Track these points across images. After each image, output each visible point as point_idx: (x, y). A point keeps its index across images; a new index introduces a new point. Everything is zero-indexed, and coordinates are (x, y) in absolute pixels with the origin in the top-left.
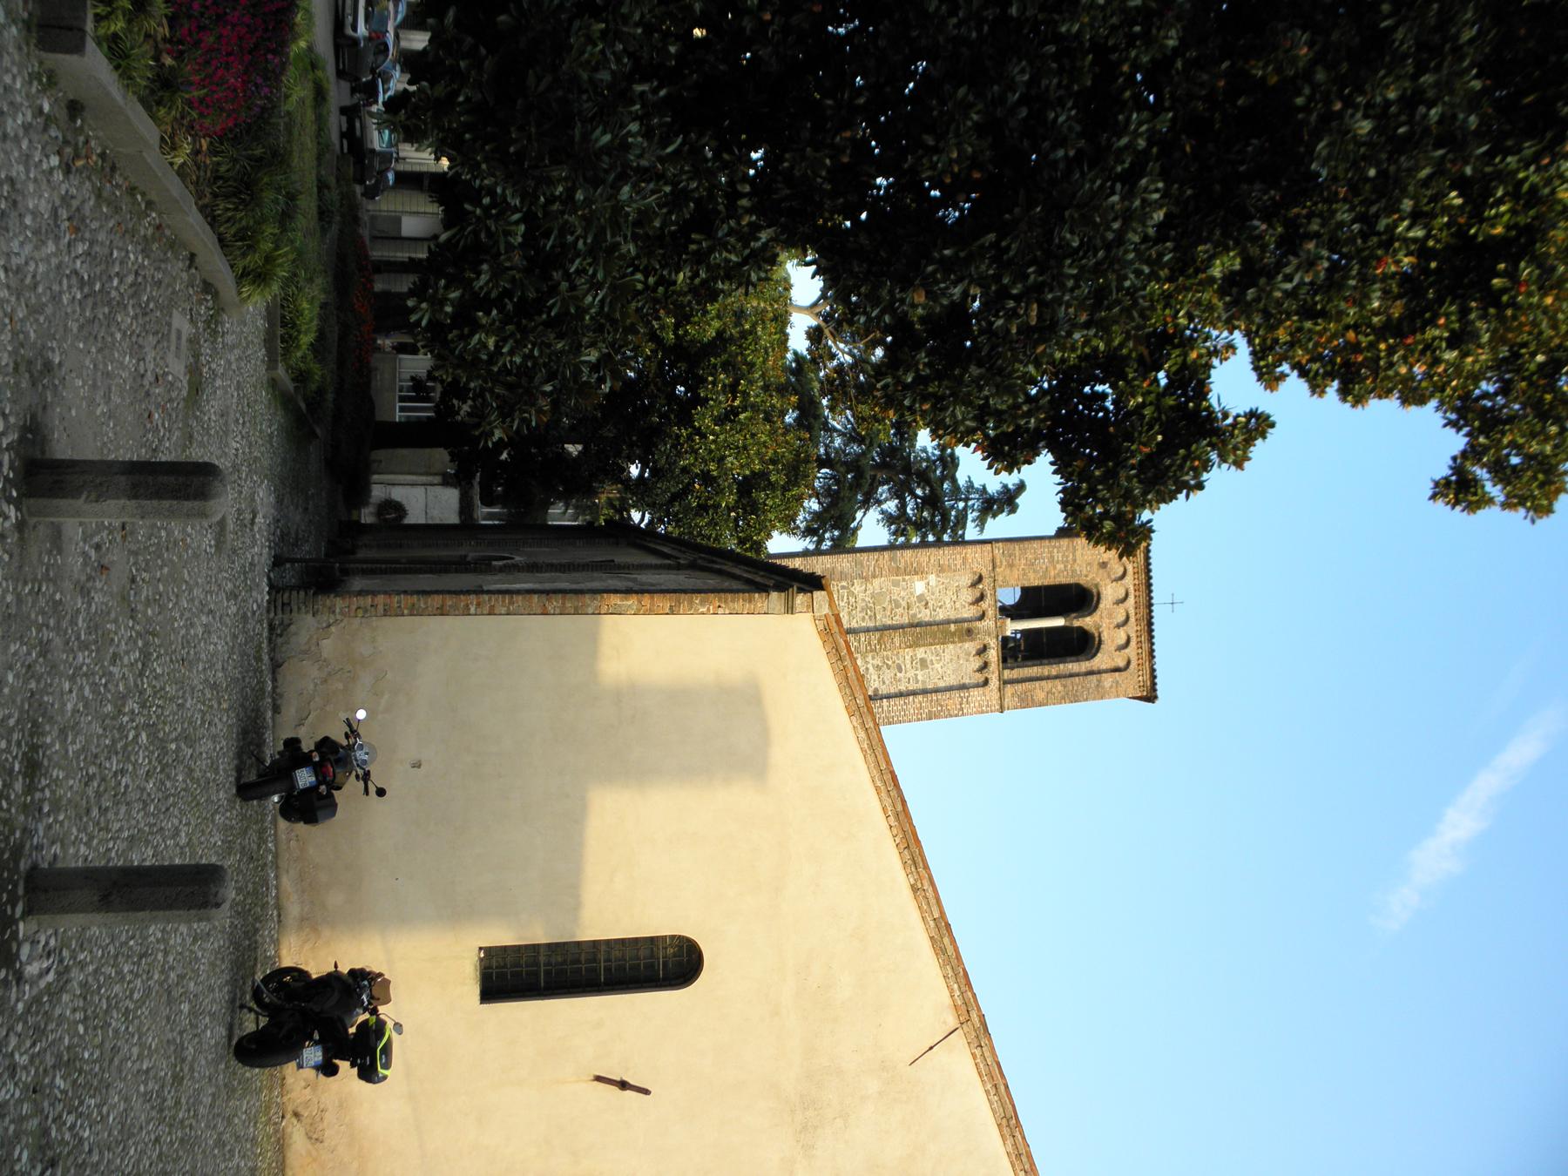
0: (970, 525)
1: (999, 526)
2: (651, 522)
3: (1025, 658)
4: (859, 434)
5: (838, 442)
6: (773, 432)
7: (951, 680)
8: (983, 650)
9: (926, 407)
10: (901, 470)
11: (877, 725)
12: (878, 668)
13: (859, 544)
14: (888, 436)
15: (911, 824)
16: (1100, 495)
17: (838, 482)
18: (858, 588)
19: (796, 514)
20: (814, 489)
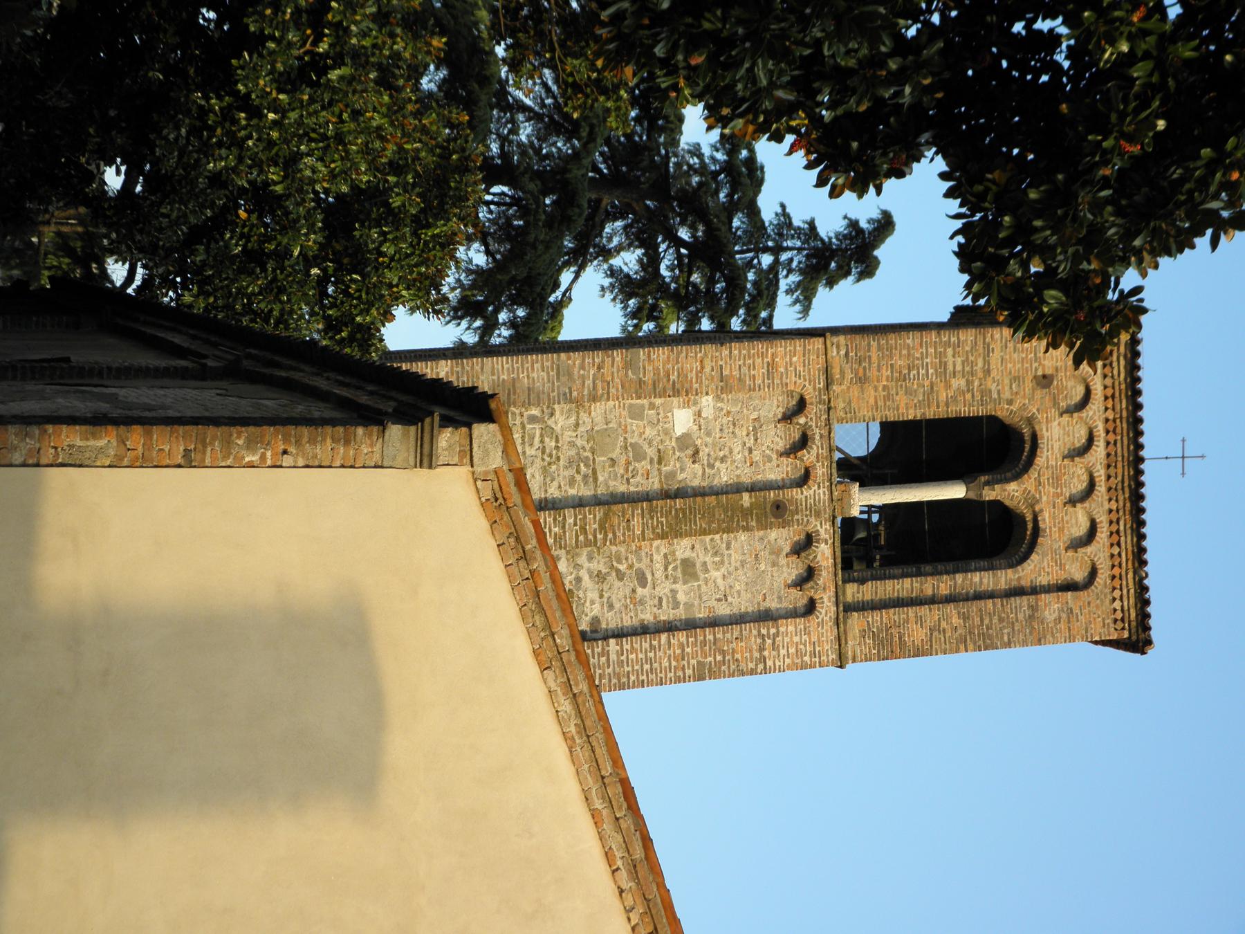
0: (783, 300)
1: (840, 303)
2: (146, 282)
3: (888, 562)
4: (567, 117)
5: (526, 132)
6: (396, 110)
7: (743, 603)
8: (805, 544)
9: (697, 60)
10: (652, 192)
11: (595, 689)
12: (600, 577)
13: (565, 335)
14: (624, 121)
15: (661, 885)
16: (1038, 238)
17: (524, 212)
18: (561, 420)
19: (441, 274)
20: (476, 223)
